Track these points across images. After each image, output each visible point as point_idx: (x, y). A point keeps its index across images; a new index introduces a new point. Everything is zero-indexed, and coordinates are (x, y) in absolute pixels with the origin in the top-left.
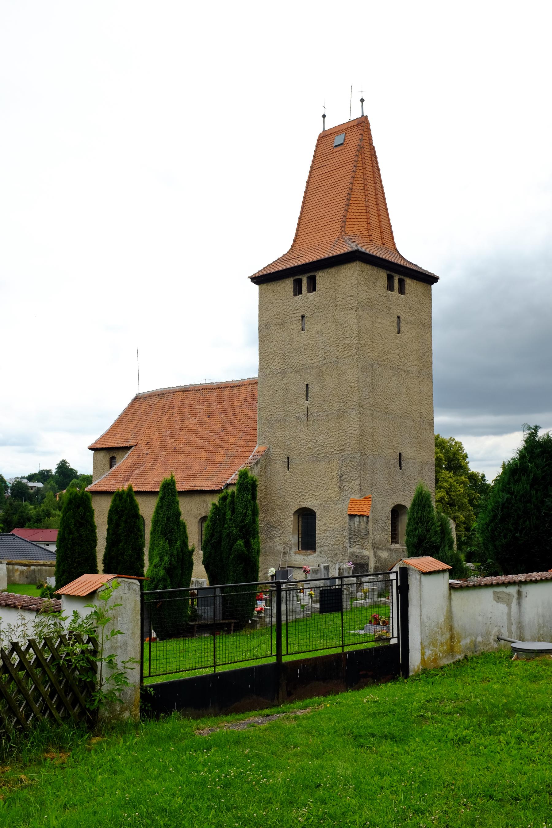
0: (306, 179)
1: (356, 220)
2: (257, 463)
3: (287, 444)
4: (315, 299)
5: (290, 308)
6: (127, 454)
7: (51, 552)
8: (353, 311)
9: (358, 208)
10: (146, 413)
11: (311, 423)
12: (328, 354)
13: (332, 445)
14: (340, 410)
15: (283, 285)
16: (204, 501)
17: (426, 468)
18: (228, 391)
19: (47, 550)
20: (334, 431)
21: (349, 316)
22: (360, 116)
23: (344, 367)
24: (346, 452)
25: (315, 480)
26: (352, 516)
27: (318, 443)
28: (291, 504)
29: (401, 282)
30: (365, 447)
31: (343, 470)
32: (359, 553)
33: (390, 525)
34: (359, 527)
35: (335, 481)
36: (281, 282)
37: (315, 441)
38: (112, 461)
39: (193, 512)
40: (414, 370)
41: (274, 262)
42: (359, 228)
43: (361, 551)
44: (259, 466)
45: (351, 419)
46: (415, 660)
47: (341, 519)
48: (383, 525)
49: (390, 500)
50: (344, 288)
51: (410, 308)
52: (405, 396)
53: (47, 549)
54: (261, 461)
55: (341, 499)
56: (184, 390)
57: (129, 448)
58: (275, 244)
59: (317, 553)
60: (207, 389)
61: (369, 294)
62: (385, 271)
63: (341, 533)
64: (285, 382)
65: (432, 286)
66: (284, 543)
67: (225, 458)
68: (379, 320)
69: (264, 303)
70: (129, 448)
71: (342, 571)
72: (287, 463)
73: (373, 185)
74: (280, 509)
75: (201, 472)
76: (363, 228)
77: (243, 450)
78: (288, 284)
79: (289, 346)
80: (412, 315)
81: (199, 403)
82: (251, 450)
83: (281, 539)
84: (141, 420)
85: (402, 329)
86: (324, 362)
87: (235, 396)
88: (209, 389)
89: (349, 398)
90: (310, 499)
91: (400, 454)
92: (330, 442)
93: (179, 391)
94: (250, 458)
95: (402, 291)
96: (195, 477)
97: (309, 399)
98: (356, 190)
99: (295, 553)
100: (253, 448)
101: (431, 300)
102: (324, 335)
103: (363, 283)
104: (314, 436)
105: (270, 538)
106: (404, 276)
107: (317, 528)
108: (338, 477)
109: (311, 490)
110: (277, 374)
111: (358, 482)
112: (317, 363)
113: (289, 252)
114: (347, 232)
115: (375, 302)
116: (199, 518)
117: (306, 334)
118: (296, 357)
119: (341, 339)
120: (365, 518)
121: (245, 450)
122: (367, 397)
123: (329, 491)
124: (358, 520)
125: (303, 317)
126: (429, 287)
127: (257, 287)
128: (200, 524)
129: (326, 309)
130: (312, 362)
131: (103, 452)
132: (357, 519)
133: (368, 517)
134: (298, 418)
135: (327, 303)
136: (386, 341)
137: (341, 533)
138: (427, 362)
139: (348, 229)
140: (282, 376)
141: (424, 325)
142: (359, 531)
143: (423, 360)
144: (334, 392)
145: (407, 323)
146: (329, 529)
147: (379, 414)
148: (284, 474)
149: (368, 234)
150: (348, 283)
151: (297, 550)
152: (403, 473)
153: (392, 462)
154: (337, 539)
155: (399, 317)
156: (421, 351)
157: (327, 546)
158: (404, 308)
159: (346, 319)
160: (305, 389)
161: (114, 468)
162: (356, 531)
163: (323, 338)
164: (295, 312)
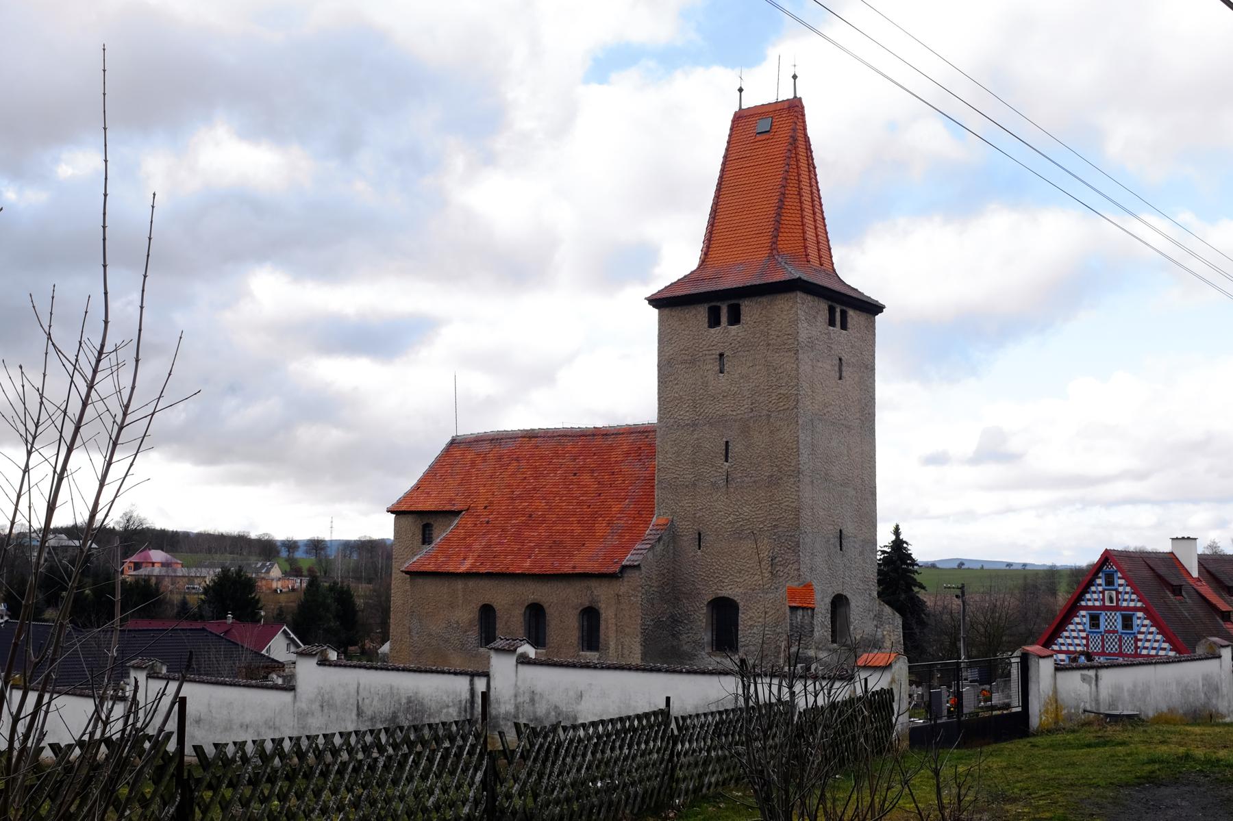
2: (659, 540)
8: (792, 354)
10: (473, 463)
15: (694, 312)
16: (588, 588)
18: (598, 441)
22: (791, 97)
29: (844, 314)
46: (1034, 722)
58: (679, 257)
68: (820, 364)
82: (647, 523)
85: (844, 374)
87: (611, 448)
95: (844, 326)
99: (709, 654)
105: (674, 635)
107: (740, 622)
125: (721, 355)
127: (656, 311)
132: (800, 612)
134: (713, 484)
153: (832, 541)
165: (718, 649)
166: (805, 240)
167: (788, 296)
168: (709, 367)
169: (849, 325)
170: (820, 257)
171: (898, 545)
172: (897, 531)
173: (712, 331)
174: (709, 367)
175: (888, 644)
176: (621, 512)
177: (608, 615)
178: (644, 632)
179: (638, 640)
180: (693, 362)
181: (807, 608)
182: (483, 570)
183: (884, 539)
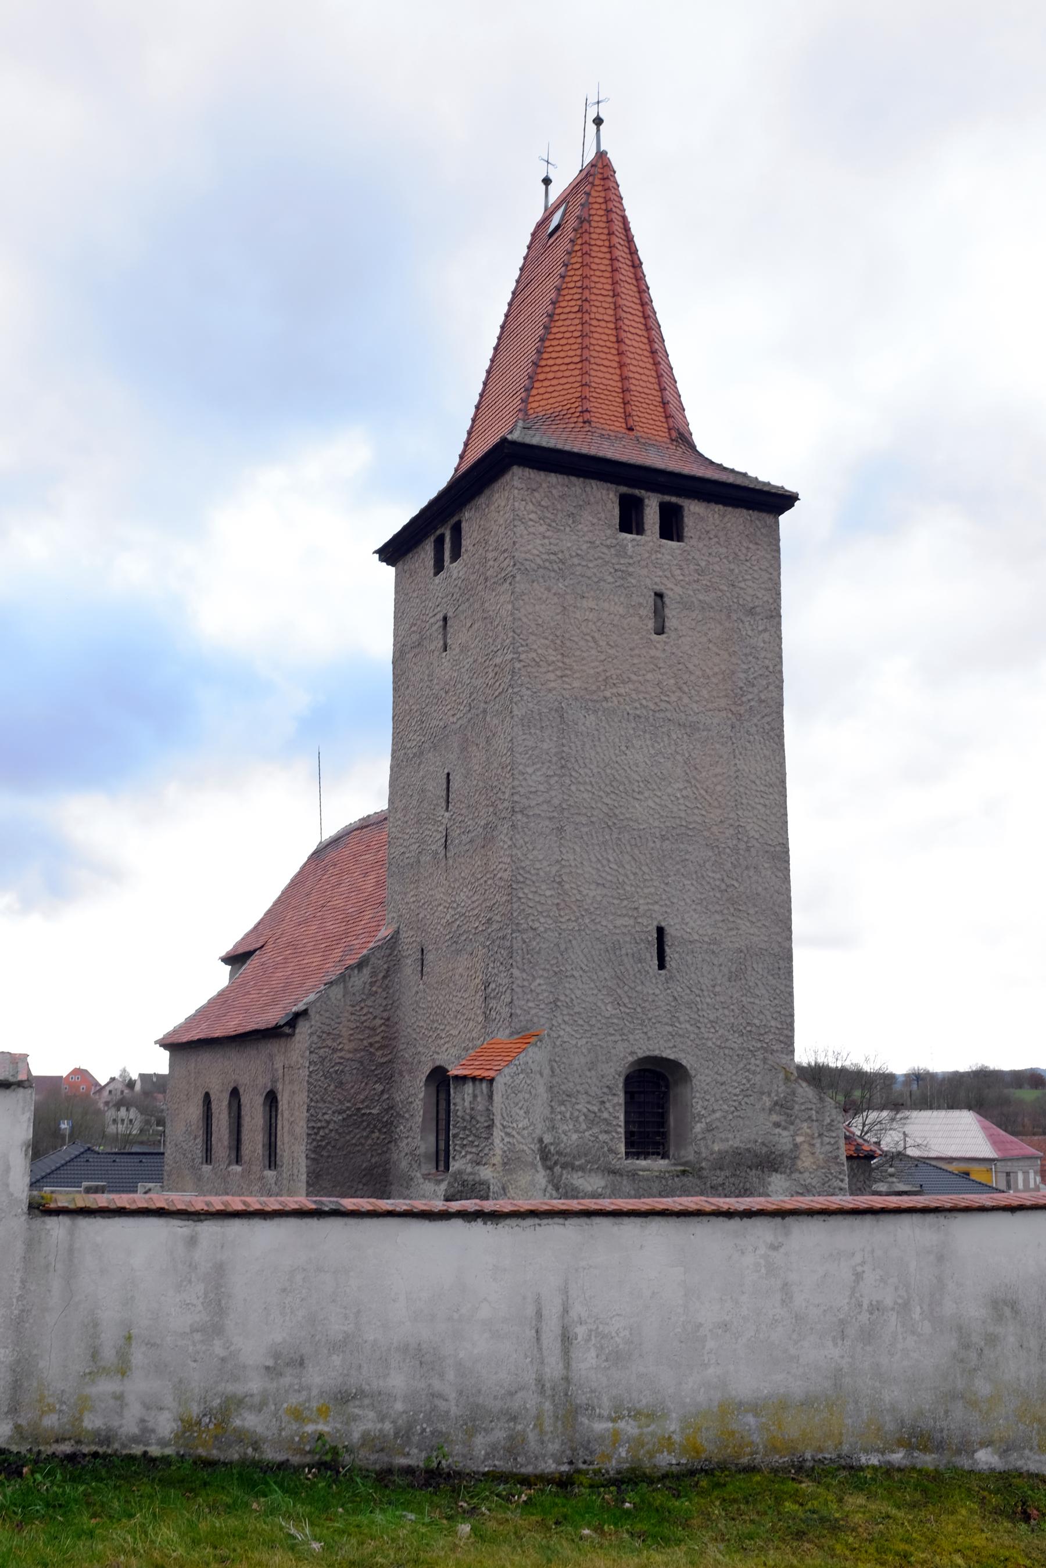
9: (562, 354)
32: (471, 1174)
34: (472, 1109)
40: (715, 721)
43: (477, 1168)
44: (366, 971)
49: (620, 1046)
51: (701, 572)
54: (373, 960)
62: (614, 487)
65: (782, 518)
73: (610, 299)
85: (671, 623)
91: (660, 931)
99: (426, 1177)
101: (778, 551)
103: (533, 516)
115: (576, 561)
120: (484, 1085)
122: (541, 788)
124: (471, 1091)
126: (768, 518)
127: (392, 570)
128: (268, 1108)
133: (491, 1081)
136: (612, 652)
138: (762, 701)
142: (472, 1118)
145: (687, 606)
147: (585, 829)
149: (579, 409)
151: (434, 1171)
155: (659, 595)
156: (742, 676)
162: (468, 1117)
175: (806, 1161)
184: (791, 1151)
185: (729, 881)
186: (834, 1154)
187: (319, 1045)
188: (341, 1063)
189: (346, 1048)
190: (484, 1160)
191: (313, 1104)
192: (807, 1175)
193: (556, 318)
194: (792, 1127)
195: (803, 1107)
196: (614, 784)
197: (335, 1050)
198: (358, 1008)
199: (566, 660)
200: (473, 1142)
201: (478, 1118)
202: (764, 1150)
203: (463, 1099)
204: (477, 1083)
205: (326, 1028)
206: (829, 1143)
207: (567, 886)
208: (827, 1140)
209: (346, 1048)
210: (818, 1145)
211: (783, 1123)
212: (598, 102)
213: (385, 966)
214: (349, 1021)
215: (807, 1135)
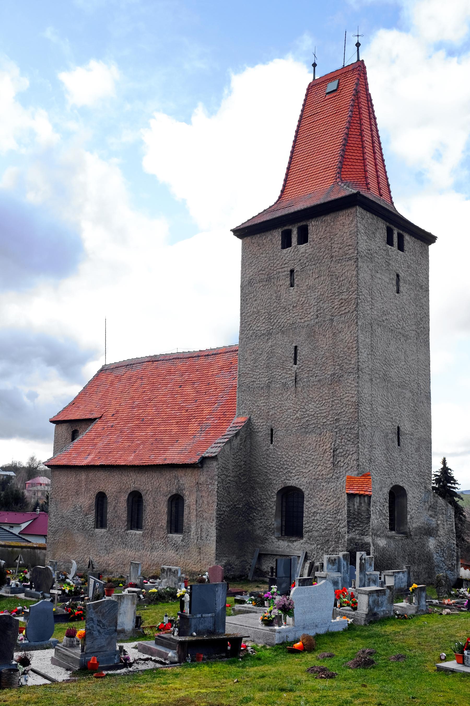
0: (295, 128)
1: (352, 167)
2: (237, 435)
3: (270, 413)
4: (307, 251)
5: (278, 262)
6: (91, 427)
7: (15, 535)
10: (112, 383)
11: (300, 389)
12: (322, 311)
13: (325, 414)
14: (334, 374)
17: (423, 446)
18: (201, 361)
19: (11, 533)
20: (327, 398)
21: (347, 268)
22: (355, 60)
23: (341, 325)
24: (341, 423)
25: (304, 455)
26: (351, 496)
27: (308, 412)
28: (275, 482)
29: (401, 238)
30: (363, 417)
31: (337, 442)
32: (359, 539)
33: (388, 508)
35: (328, 455)
36: (268, 234)
37: (304, 410)
38: (74, 435)
39: (161, 489)
41: (259, 214)
42: (355, 175)
43: (362, 537)
44: (238, 438)
45: (348, 384)
47: (334, 499)
48: (381, 508)
50: (342, 236)
52: (403, 363)
53: (11, 531)
54: (241, 432)
55: (334, 477)
56: (153, 360)
57: (92, 421)
58: (262, 193)
59: (304, 539)
60: (178, 358)
61: (369, 245)
63: (334, 516)
64: (270, 344)
65: (430, 247)
66: (265, 527)
67: (199, 429)
68: (378, 275)
69: (247, 257)
70: (92, 421)
71: (363, 561)
72: (270, 436)
74: (261, 488)
75: (172, 445)
76: (360, 175)
77: (219, 421)
78: (276, 236)
79: (275, 304)
80: (411, 275)
81: (169, 372)
82: (229, 421)
83: (261, 522)
84: (107, 391)
85: (401, 289)
86: (316, 320)
88: (181, 358)
89: (345, 361)
90: (297, 477)
91: (398, 428)
92: (322, 411)
93: (149, 361)
94: (227, 429)
95: (401, 248)
96: (166, 450)
97: (298, 363)
98: (353, 136)
99: (278, 538)
100: (230, 419)
101: (428, 261)
102: (317, 291)
103: (363, 231)
104: (303, 404)
105: (249, 521)
106: (403, 231)
107: (305, 510)
108: (332, 451)
109: (298, 466)
110: (260, 336)
111: (355, 457)
112: (308, 322)
113: (276, 203)
114: (343, 179)
116: (169, 496)
117: (295, 290)
118: (283, 316)
119: (336, 294)
120: (366, 499)
121: (222, 421)
123: (320, 468)
124: (358, 501)
125: (292, 271)
128: (170, 503)
129: (320, 261)
130: (302, 321)
131: (65, 425)
132: (357, 500)
134: (284, 384)
135: (321, 254)
137: (334, 516)
139: (344, 176)
140: (267, 338)
141: (421, 287)
142: (359, 513)
143: (421, 326)
144: (327, 354)
146: (319, 511)
147: (378, 380)
148: (266, 447)
150: (347, 231)
152: (401, 450)
154: (330, 523)
155: (398, 276)
156: (419, 316)
157: (317, 531)
158: (402, 266)
159: (344, 271)
160: (293, 352)
161: (76, 441)
163: (316, 293)
164: (283, 266)
165: (286, 534)
166: (366, 171)
167: (349, 211)
168: (281, 283)
169: (406, 248)
170: (379, 189)
171: (445, 470)
172: (444, 462)
173: (285, 251)
174: (281, 283)
175: (441, 532)
176: (210, 414)
177: (190, 500)
178: (219, 517)
179: (214, 524)
180: (269, 279)
181: (364, 496)
182: (98, 463)
183: (436, 467)
184: (436, 527)
185: (416, 408)
186: (452, 529)
187: (221, 473)
188: (229, 483)
189: (231, 475)
190: (366, 534)
191: (219, 503)
192: (441, 537)
193: (350, 136)
194: (436, 517)
195: (440, 508)
196: (386, 360)
197: (227, 476)
198: (235, 456)
199: (373, 301)
200: (359, 525)
201: (363, 514)
202: (427, 527)
203: (354, 505)
204: (362, 497)
205: (224, 465)
206: (449, 524)
207: (373, 407)
208: (449, 523)
209: (231, 475)
210: (446, 525)
211: (433, 515)
212: (358, 36)
213: (245, 436)
214: (232, 462)
215: (441, 520)
